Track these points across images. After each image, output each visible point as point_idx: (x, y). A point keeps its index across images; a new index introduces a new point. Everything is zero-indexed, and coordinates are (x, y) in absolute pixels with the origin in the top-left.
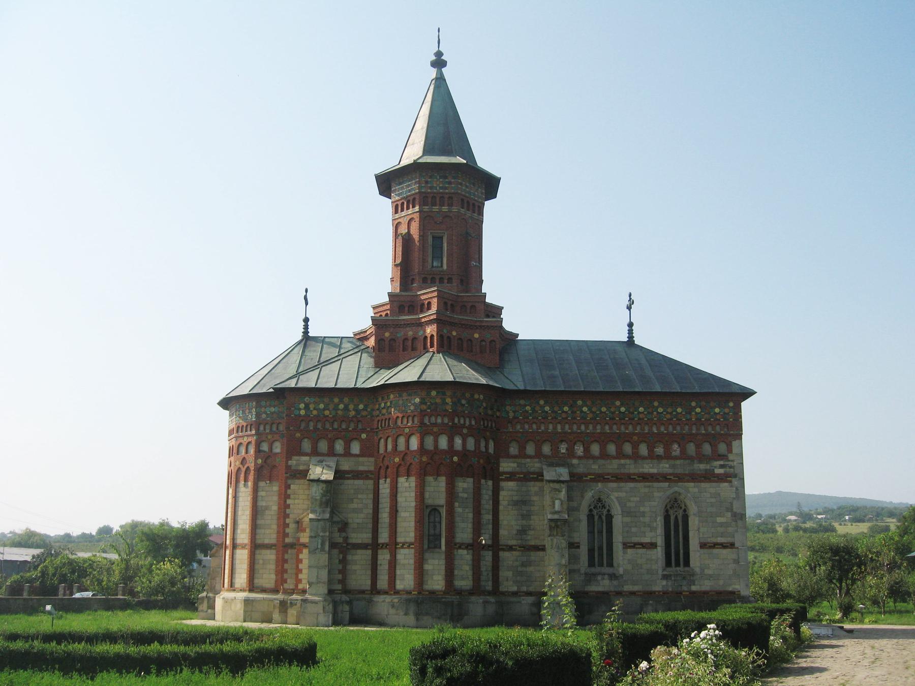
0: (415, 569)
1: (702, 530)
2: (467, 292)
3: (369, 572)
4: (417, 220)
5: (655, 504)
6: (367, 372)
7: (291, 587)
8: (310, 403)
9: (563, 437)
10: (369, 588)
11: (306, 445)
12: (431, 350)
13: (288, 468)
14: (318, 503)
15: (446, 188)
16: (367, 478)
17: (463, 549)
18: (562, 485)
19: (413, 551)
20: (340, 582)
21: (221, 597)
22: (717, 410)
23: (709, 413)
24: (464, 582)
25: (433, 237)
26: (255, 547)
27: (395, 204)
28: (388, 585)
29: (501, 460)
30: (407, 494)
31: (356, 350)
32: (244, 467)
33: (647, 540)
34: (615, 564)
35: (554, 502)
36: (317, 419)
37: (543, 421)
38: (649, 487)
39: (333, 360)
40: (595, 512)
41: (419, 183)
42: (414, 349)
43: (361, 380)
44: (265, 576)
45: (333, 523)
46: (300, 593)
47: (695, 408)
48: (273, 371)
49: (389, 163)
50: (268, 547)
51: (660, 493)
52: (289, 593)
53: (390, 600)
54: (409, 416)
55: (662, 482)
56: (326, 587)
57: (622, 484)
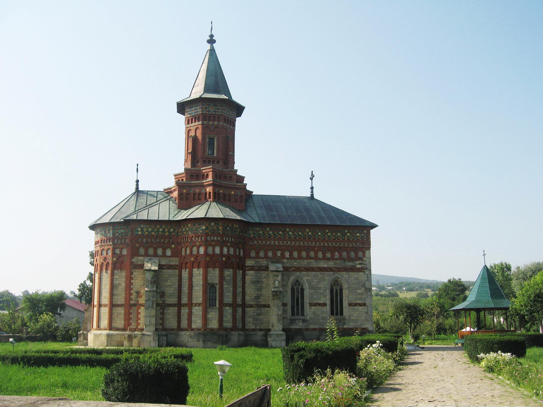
0: (203, 317)
1: (349, 297)
2: (227, 168)
3: (176, 319)
4: (201, 129)
5: (326, 283)
6: (174, 211)
7: (134, 328)
8: (144, 228)
9: (279, 248)
10: (176, 327)
11: (142, 251)
12: (209, 200)
13: (132, 263)
14: (150, 282)
15: (216, 112)
16: (175, 269)
17: (227, 306)
18: (279, 273)
19: (201, 308)
20: (161, 324)
21: (93, 333)
22: (358, 235)
23: (354, 236)
24: (228, 324)
25: (209, 138)
26: (112, 306)
27: (188, 119)
28: (188, 326)
29: (247, 259)
30: (198, 277)
31: (165, 199)
32: (105, 262)
33: (321, 302)
34: (305, 314)
35: (275, 282)
36: (148, 236)
37: (268, 239)
38: (323, 274)
39: (154, 204)
40: (295, 287)
41: (202, 108)
42: (199, 199)
43: (172, 216)
44: (118, 322)
45: (157, 293)
46: (139, 330)
47: (347, 233)
48: (121, 210)
49: (184, 96)
50: (105, 306)
51: (328, 277)
52: (132, 330)
53: (189, 334)
54: (199, 236)
55: (330, 272)
56: (154, 327)
57: (310, 273)
